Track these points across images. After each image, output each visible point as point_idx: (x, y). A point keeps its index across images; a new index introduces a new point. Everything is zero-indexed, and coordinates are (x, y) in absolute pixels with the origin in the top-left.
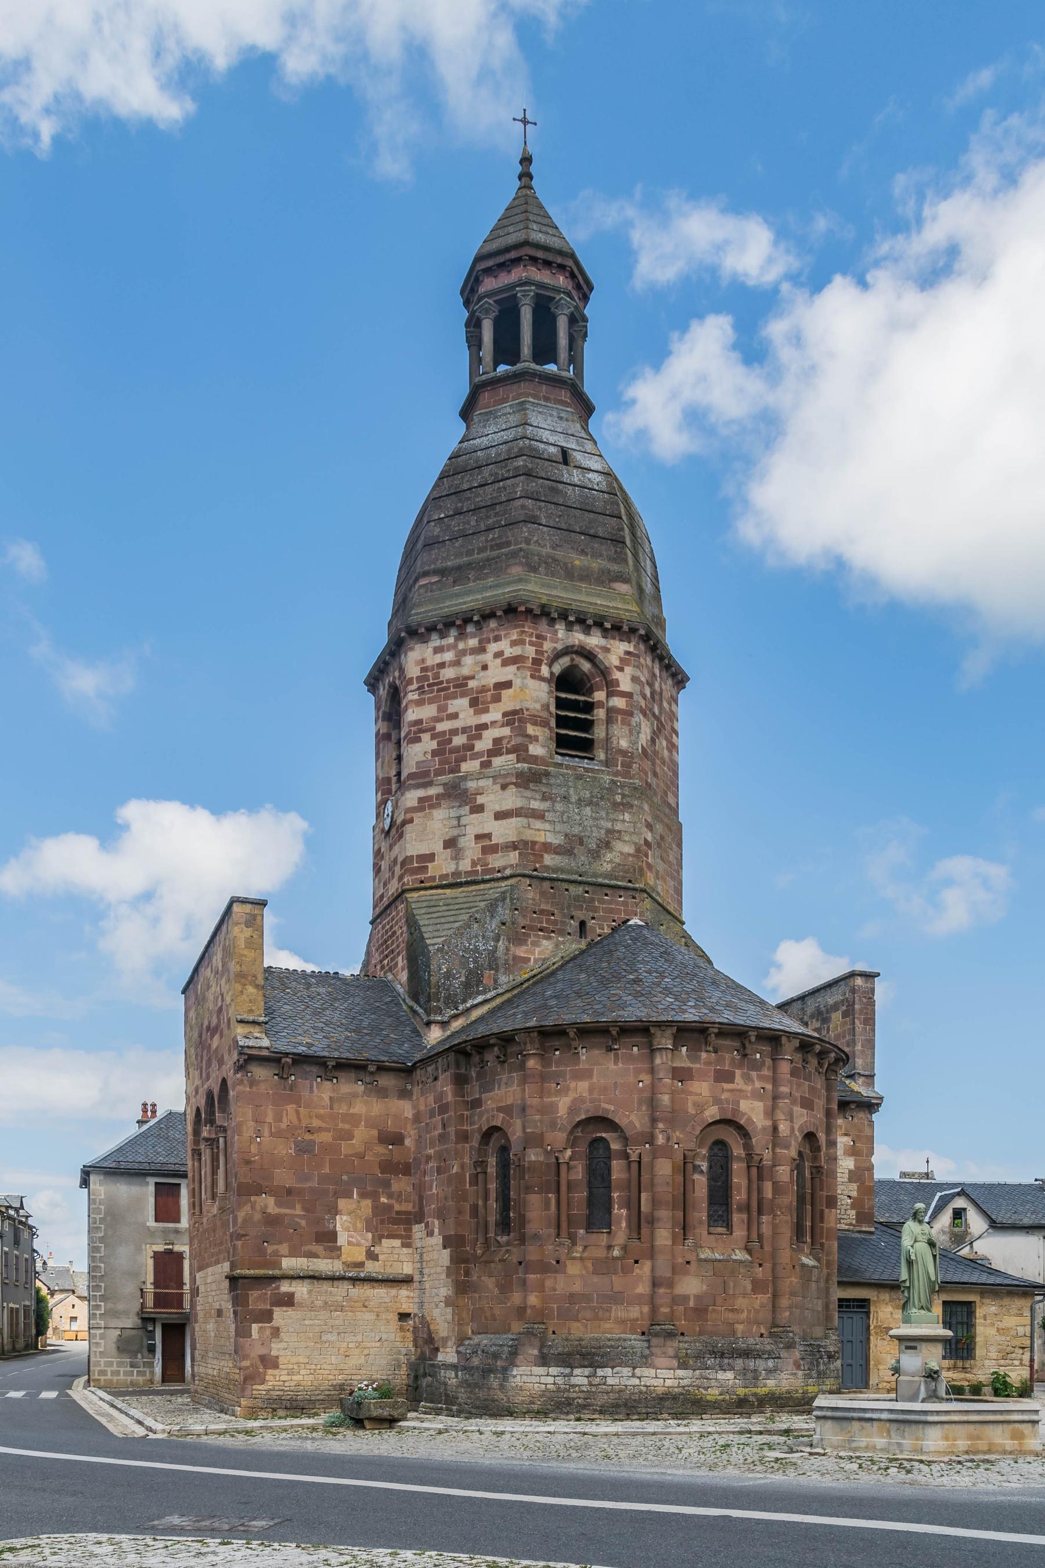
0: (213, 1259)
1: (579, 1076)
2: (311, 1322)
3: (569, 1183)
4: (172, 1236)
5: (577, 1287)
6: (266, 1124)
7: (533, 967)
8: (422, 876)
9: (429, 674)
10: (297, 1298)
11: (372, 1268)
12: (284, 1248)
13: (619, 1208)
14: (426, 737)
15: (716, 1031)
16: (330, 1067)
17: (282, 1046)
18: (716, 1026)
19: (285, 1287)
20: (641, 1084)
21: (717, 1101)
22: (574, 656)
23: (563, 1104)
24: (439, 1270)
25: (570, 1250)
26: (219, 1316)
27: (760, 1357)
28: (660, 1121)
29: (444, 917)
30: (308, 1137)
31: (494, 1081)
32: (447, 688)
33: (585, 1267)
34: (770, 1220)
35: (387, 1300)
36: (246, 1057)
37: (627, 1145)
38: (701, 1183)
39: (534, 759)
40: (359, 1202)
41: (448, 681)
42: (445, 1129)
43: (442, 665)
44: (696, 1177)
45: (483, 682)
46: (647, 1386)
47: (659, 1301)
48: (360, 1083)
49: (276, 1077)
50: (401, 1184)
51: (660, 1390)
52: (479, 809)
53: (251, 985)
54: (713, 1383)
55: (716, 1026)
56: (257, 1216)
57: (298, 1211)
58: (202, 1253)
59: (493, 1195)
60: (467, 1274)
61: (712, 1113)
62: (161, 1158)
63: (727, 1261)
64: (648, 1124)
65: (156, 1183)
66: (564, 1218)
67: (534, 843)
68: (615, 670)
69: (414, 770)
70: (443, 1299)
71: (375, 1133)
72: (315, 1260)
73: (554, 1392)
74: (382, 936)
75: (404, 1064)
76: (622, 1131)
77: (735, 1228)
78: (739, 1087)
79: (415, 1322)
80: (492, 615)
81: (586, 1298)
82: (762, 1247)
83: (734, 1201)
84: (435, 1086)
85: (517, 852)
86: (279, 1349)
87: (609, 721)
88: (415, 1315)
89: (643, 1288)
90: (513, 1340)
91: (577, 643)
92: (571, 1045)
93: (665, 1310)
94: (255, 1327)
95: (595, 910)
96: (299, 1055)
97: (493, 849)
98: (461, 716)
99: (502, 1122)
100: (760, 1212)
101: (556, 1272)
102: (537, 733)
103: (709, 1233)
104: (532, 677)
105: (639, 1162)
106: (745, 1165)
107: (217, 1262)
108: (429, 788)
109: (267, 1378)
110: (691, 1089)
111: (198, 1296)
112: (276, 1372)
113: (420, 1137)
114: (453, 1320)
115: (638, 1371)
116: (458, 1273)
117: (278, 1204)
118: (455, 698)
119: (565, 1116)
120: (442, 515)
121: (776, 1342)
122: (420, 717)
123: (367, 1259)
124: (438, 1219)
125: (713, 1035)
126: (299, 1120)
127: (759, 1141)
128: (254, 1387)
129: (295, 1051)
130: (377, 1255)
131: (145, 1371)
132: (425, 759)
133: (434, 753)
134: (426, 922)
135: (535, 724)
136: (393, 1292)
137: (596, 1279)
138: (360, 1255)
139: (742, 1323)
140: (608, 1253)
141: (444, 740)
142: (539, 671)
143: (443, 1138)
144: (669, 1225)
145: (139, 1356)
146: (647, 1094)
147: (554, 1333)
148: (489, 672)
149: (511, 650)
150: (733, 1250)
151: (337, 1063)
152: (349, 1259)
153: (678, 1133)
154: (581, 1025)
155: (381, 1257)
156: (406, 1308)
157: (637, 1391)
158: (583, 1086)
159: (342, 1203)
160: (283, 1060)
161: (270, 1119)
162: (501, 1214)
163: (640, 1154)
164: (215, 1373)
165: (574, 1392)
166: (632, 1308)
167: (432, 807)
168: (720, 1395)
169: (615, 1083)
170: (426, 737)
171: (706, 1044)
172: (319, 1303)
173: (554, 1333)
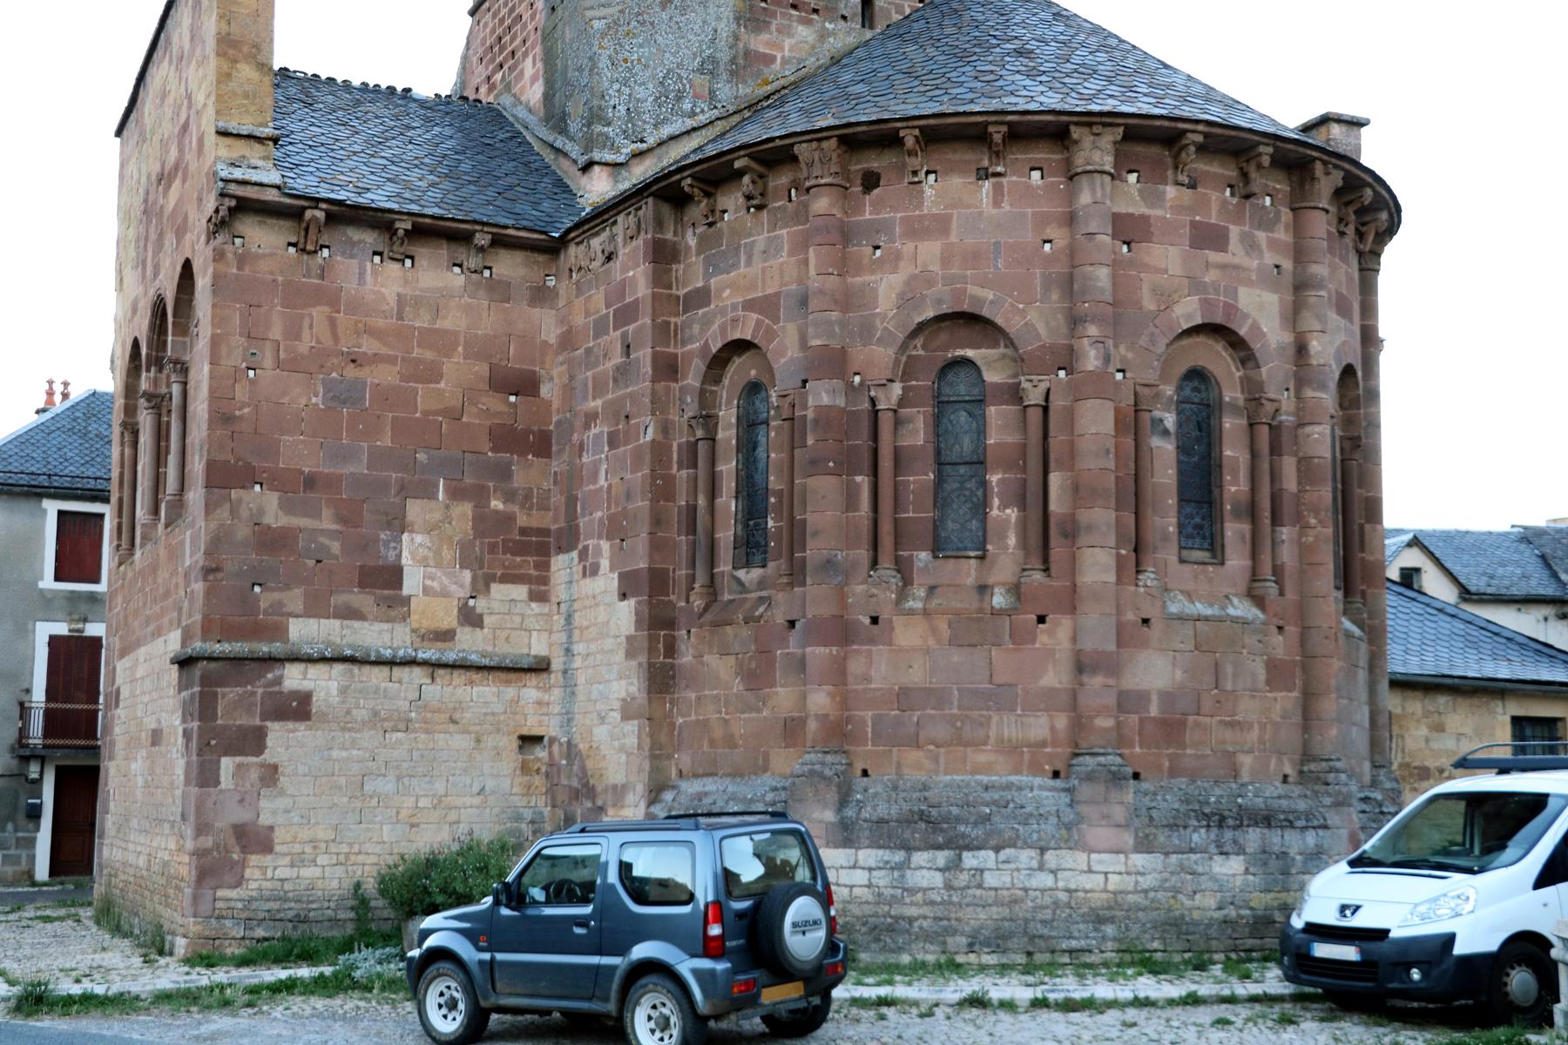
0: (151, 628)
1: (918, 230)
2: (344, 754)
3: (897, 453)
4: (83, 608)
5: (916, 675)
6: (268, 343)
7: (780, 72)
10: (317, 704)
11: (469, 643)
12: (294, 599)
13: (1003, 507)
15: (1199, 138)
16: (401, 232)
17: (305, 184)
18: (1201, 127)
19: (294, 678)
20: (1047, 247)
21: (1196, 286)
24: (609, 643)
25: (902, 595)
26: (154, 744)
27: (1291, 825)
28: (1093, 322)
30: (351, 372)
31: (737, 249)
33: (934, 631)
34: (1295, 536)
35: (498, 708)
36: (233, 203)
38: (1164, 451)
40: (447, 507)
42: (628, 355)
44: (1156, 442)
46: (1068, 891)
47: (1087, 701)
48: (457, 270)
49: (292, 250)
51: (1098, 899)
53: (247, 62)
54: (1206, 883)
55: (1201, 127)
56: (243, 532)
57: (327, 522)
58: (130, 620)
59: (728, 485)
60: (671, 650)
61: (1188, 311)
62: (71, 468)
63: (1220, 620)
64: (1064, 330)
65: (61, 513)
66: (886, 528)
70: (617, 705)
71: (483, 369)
72: (357, 624)
73: (867, 903)
74: (493, 31)
75: (545, 233)
76: (1010, 343)
77: (1228, 550)
78: (1236, 261)
79: (550, 753)
81: (937, 697)
82: (1282, 593)
83: (1226, 496)
84: (608, 272)
86: (274, 813)
88: (552, 740)
89: (1055, 677)
90: (774, 789)
92: (904, 165)
93: (1105, 722)
94: (227, 764)
96: (340, 203)
99: (756, 330)
100: (1276, 520)
101: (872, 641)
103: (1182, 561)
105: (1046, 409)
106: (1244, 422)
107: (158, 633)
109: (248, 873)
110: (1147, 259)
111: (117, 705)
112: (267, 860)
113: (572, 378)
114: (640, 747)
115: (1051, 858)
116: (652, 650)
117: (287, 507)
119: (891, 314)
121: (1316, 793)
123: (461, 624)
124: (608, 538)
125: (1192, 149)
127: (1274, 371)
128: (220, 893)
129: (333, 196)
130: (481, 616)
131: (19, 857)
136: (510, 692)
137: (957, 656)
138: (449, 620)
139: (1250, 751)
140: (982, 600)
143: (623, 374)
144: (1112, 541)
145: (10, 826)
146: (1060, 268)
147: (865, 773)
150: (1227, 597)
152: (426, 624)
153: (1122, 349)
155: (487, 620)
157: (1047, 900)
158: (929, 251)
159: (415, 510)
160: (308, 214)
161: (276, 332)
162: (746, 526)
163: (1049, 390)
164: (142, 862)
165: (912, 904)
166: (1032, 720)
168: (1220, 908)
169: (997, 244)
171: (1176, 167)
172: (361, 714)
173: (865, 773)
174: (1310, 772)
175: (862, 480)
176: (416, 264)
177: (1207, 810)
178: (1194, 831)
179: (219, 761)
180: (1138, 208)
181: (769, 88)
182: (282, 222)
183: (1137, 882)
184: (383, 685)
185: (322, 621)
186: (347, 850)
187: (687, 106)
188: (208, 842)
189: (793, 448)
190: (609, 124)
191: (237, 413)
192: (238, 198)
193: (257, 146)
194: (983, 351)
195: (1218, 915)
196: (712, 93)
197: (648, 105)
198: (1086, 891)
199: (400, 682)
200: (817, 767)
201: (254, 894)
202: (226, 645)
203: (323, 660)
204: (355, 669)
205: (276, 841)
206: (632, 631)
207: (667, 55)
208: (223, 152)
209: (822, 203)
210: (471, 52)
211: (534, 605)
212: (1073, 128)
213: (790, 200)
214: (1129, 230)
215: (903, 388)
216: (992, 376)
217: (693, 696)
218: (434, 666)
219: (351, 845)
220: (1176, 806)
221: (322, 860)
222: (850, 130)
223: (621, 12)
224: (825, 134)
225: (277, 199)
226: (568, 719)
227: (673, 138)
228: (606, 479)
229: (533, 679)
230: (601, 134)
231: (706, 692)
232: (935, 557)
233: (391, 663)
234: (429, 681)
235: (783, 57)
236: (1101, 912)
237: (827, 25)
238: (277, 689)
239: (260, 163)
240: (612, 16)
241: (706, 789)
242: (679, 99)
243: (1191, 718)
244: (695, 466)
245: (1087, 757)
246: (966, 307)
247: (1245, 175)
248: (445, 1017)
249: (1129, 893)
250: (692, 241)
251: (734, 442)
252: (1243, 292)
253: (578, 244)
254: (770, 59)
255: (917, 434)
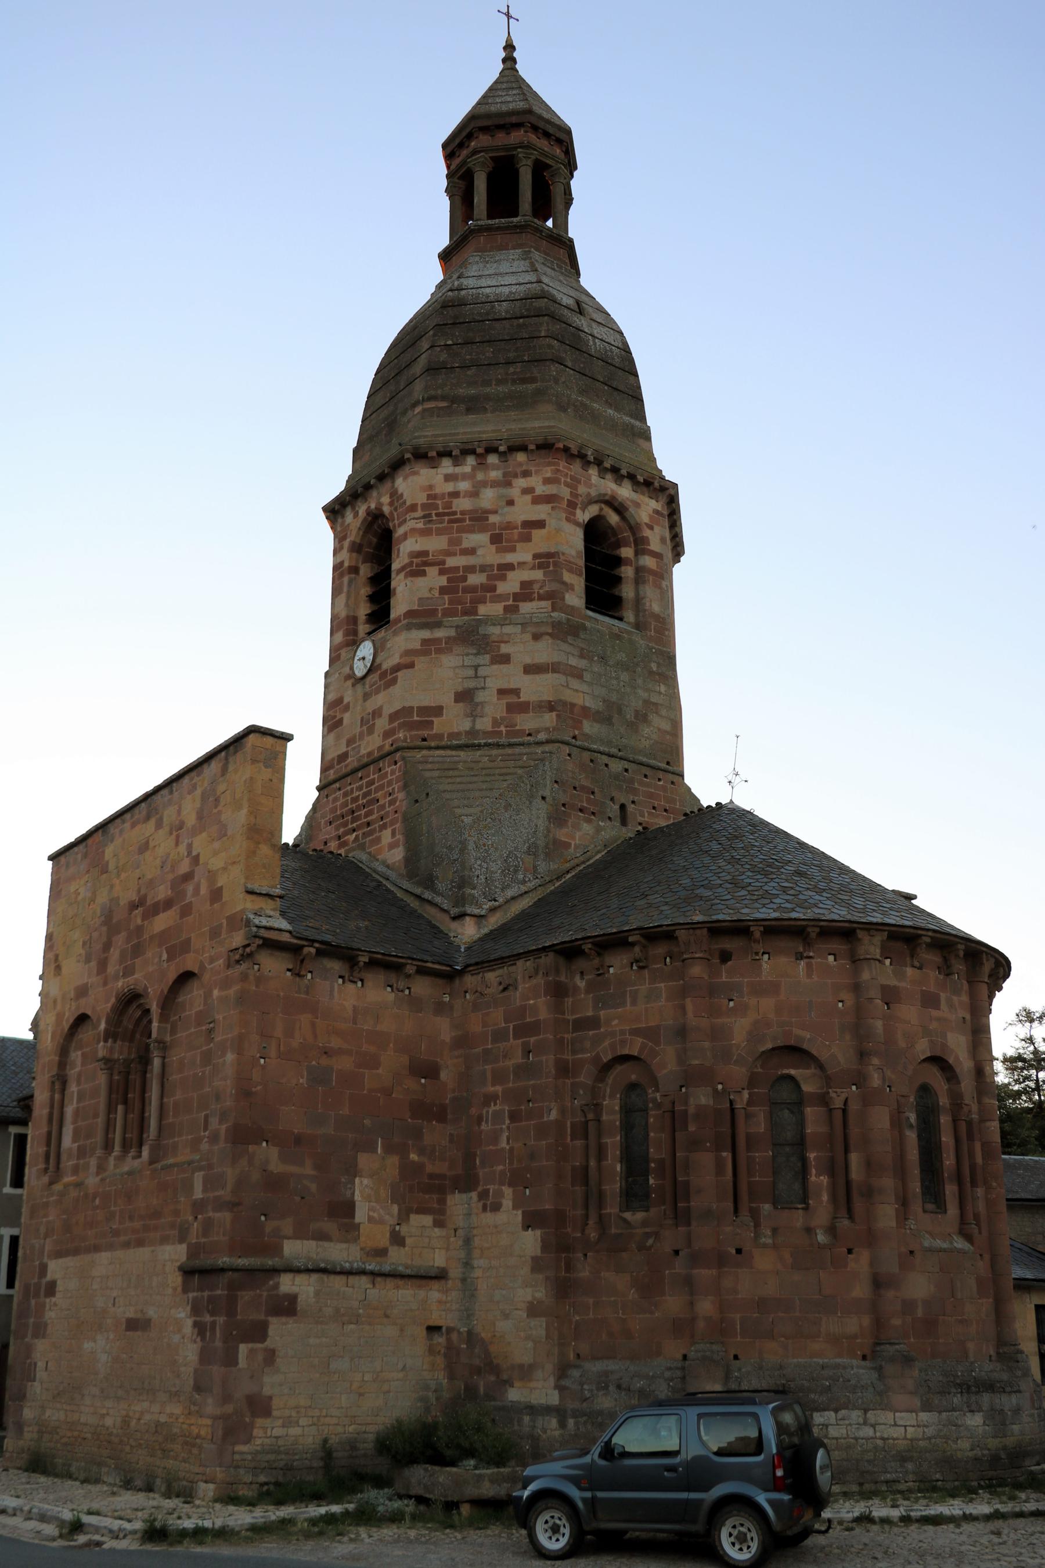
3: (748, 1136)
8: (425, 733)
9: (439, 502)
11: (398, 1259)
12: (287, 1226)
13: (818, 1175)
14: (432, 571)
15: (928, 940)
16: (362, 964)
18: (930, 934)
19: (287, 1284)
20: (840, 1005)
22: (603, 506)
23: (740, 1028)
25: (757, 1236)
29: (470, 783)
30: (324, 1061)
32: (463, 520)
37: (829, 1086)
39: (571, 610)
40: (383, 1158)
41: (463, 513)
43: (456, 494)
45: (509, 518)
48: (389, 989)
49: (289, 974)
50: (435, 1135)
52: (505, 659)
55: (930, 934)
57: (309, 1171)
60: (569, 1268)
61: (923, 1048)
67: (573, 705)
68: (645, 527)
69: (416, 608)
72: (326, 1244)
76: (821, 1067)
79: (449, 1340)
80: (523, 448)
82: (980, 1233)
85: (554, 714)
87: (639, 580)
88: (450, 1330)
89: (861, 1291)
90: (669, 1369)
91: (609, 492)
94: (243, 1348)
95: (635, 792)
97: (524, 708)
98: (479, 552)
100: (974, 1183)
102: (573, 582)
104: (568, 519)
105: (844, 1111)
108: (436, 630)
109: (255, 1432)
114: (548, 1337)
118: (472, 532)
120: (450, 342)
122: (426, 548)
123: (392, 1244)
124: (510, 1185)
126: (315, 1036)
130: (404, 1238)
132: (430, 596)
133: (443, 590)
134: (449, 787)
135: (570, 571)
136: (422, 1293)
138: (382, 1239)
141: (455, 579)
142: (574, 514)
147: (736, 1357)
148: (515, 509)
149: (544, 488)
151: (370, 959)
154: (598, 939)
155: (408, 1241)
156: (435, 1320)
158: (767, 1004)
159: (364, 1160)
160: (306, 950)
162: (627, 1181)
167: (439, 651)
168: (972, 1450)
170: (432, 571)
171: (912, 956)
173: (736, 1357)
174: (1005, 1353)
175: (727, 1155)
176: (365, 985)
177: (958, 1381)
178: (954, 1396)
179: (238, 1348)
180: (893, 982)
181: (568, 865)
182: (284, 954)
183: (924, 1432)
184: (343, 1289)
185: (305, 1242)
186: (318, 1414)
187: (520, 877)
188: (229, 1408)
189: (674, 1131)
190: (474, 888)
191: (254, 1089)
192: (264, 939)
193: (270, 901)
194: (801, 1070)
195: (970, 1454)
196: (535, 867)
197: (497, 876)
198: (894, 1439)
199: (353, 1287)
200: (708, 1354)
201: (259, 1448)
202: (245, 1260)
203: (308, 1271)
204: (325, 1277)
205: (274, 1407)
206: (539, 1253)
207: (509, 842)
208: (249, 905)
209: (696, 970)
210: (318, 815)
211: (436, 1230)
212: (858, 931)
213: (666, 964)
214: (890, 996)
215: (749, 1094)
216: (807, 1088)
217: (591, 1301)
218: (374, 1274)
219: (321, 1410)
220: (941, 1378)
221: (303, 1421)
222: (718, 925)
223: (482, 812)
224: (699, 926)
225: (289, 940)
226: (468, 1314)
227: (513, 898)
228: (508, 1143)
229: (436, 1285)
230: (470, 894)
231: (604, 1299)
232: (776, 1208)
233: (349, 1273)
234: (371, 1286)
235: (575, 845)
236: (904, 1454)
237: (600, 823)
238: (275, 1292)
239: (272, 913)
240: (476, 814)
241: (609, 1368)
242: (516, 871)
243: (941, 1318)
244: (586, 1138)
245: (888, 1346)
246: (792, 1042)
247: (945, 959)
248: (550, 1538)
249: (920, 1440)
250: (581, 984)
251: (618, 1123)
252: (949, 1035)
253: (472, 975)
254: (567, 845)
255: (760, 1125)
